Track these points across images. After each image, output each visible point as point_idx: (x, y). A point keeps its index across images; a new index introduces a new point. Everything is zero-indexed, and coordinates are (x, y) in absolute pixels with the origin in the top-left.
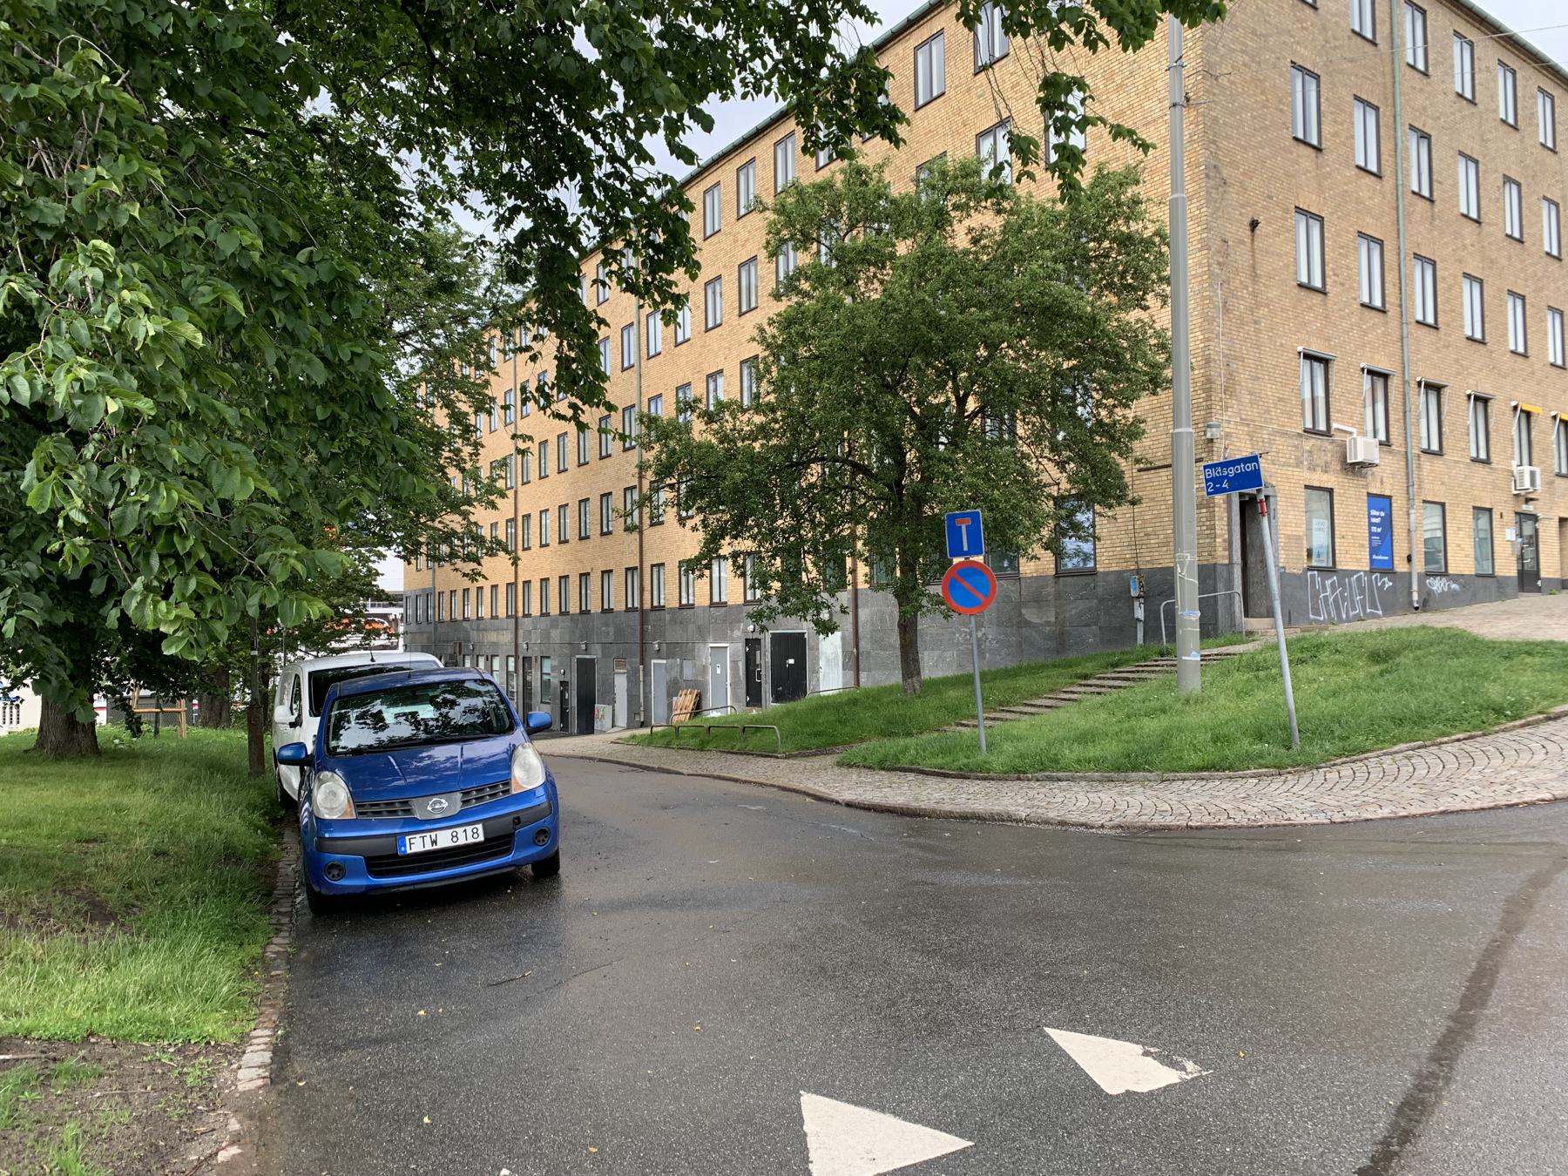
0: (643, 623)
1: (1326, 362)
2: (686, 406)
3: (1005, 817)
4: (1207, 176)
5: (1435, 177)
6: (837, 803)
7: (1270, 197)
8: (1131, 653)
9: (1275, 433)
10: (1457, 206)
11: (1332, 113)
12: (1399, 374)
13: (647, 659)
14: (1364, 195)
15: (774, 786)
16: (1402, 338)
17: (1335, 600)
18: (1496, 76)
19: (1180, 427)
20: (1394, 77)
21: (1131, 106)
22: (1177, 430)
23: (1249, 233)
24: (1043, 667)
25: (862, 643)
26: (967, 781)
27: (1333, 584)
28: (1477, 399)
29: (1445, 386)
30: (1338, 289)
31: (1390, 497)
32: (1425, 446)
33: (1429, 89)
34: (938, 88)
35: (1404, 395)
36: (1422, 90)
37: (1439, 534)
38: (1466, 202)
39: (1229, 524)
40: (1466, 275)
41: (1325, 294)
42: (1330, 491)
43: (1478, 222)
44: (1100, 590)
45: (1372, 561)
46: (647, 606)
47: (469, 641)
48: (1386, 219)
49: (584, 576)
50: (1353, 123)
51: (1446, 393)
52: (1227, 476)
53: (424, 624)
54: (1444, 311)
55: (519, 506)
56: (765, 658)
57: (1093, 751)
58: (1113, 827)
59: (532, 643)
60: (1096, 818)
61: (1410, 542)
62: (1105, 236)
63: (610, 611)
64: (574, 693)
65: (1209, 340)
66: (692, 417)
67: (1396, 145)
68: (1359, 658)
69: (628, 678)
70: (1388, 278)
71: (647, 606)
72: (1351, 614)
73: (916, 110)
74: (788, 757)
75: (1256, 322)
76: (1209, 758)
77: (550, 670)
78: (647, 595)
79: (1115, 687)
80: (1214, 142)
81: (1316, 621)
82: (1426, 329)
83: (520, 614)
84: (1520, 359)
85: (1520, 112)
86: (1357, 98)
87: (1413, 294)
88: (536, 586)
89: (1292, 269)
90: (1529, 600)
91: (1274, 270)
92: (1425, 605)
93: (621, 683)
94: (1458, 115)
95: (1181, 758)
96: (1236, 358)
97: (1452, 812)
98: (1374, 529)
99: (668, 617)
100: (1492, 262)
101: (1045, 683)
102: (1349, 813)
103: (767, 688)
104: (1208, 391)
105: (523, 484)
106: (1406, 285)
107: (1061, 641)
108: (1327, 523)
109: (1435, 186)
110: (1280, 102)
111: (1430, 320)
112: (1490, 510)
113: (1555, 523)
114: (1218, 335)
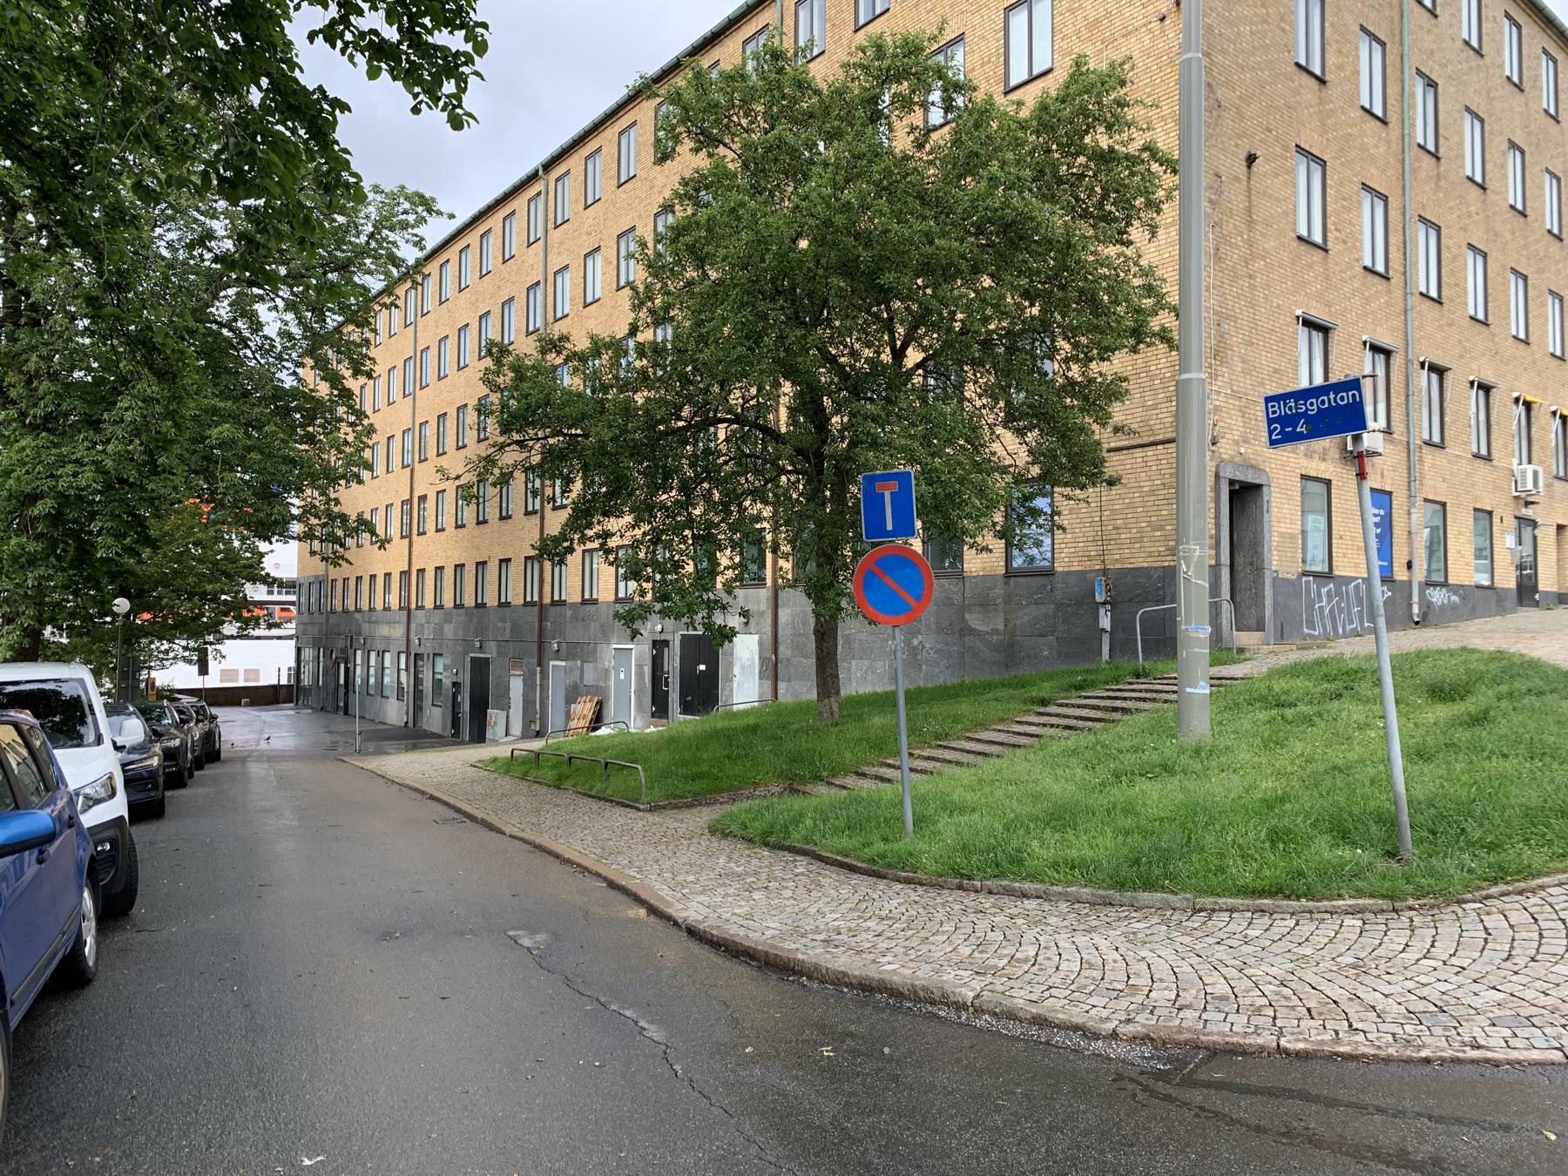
0: (542, 618)
1: (1325, 330)
2: (552, 345)
3: (937, 995)
5: (1441, 131)
6: (676, 923)
7: (1270, 131)
8: (1097, 671)
11: (1336, 41)
12: (1402, 352)
13: (545, 659)
14: (1370, 141)
15: (598, 875)
16: (1406, 311)
17: (1332, 611)
18: (1502, 28)
21: (1108, 14)
23: (1245, 169)
24: (989, 686)
25: (781, 649)
26: (882, 884)
27: (1329, 592)
28: (1481, 386)
29: (1448, 369)
30: (1341, 247)
31: (1390, 493)
32: (1426, 437)
34: (882, 4)
35: (1407, 377)
36: (1429, 31)
38: (1471, 166)
39: (1217, 517)
40: (1471, 246)
41: (1326, 251)
42: (1328, 483)
43: (1483, 188)
44: (1058, 595)
46: (547, 600)
47: (360, 634)
48: (1391, 172)
49: (481, 565)
50: (1358, 57)
51: (1449, 376)
52: (1305, 414)
53: (316, 614)
54: (1448, 284)
55: (415, 486)
56: (673, 662)
57: (1079, 849)
58: (1133, 1039)
59: (426, 633)
60: (1099, 1012)
61: (1410, 545)
62: (1081, 150)
63: (507, 604)
64: (467, 695)
66: (553, 359)
69: (524, 681)
70: (1392, 240)
71: (547, 600)
73: (856, 31)
74: (653, 809)
75: (1250, 277)
77: (443, 670)
78: (547, 588)
82: (1429, 303)
83: (413, 606)
84: (1522, 346)
85: (1525, 71)
90: (1528, 617)
93: (516, 686)
94: (1465, 65)
95: (1221, 870)
99: (569, 613)
100: (1496, 235)
101: (996, 710)
107: (1010, 651)
108: (1323, 519)
112: (1490, 513)
113: (1553, 530)
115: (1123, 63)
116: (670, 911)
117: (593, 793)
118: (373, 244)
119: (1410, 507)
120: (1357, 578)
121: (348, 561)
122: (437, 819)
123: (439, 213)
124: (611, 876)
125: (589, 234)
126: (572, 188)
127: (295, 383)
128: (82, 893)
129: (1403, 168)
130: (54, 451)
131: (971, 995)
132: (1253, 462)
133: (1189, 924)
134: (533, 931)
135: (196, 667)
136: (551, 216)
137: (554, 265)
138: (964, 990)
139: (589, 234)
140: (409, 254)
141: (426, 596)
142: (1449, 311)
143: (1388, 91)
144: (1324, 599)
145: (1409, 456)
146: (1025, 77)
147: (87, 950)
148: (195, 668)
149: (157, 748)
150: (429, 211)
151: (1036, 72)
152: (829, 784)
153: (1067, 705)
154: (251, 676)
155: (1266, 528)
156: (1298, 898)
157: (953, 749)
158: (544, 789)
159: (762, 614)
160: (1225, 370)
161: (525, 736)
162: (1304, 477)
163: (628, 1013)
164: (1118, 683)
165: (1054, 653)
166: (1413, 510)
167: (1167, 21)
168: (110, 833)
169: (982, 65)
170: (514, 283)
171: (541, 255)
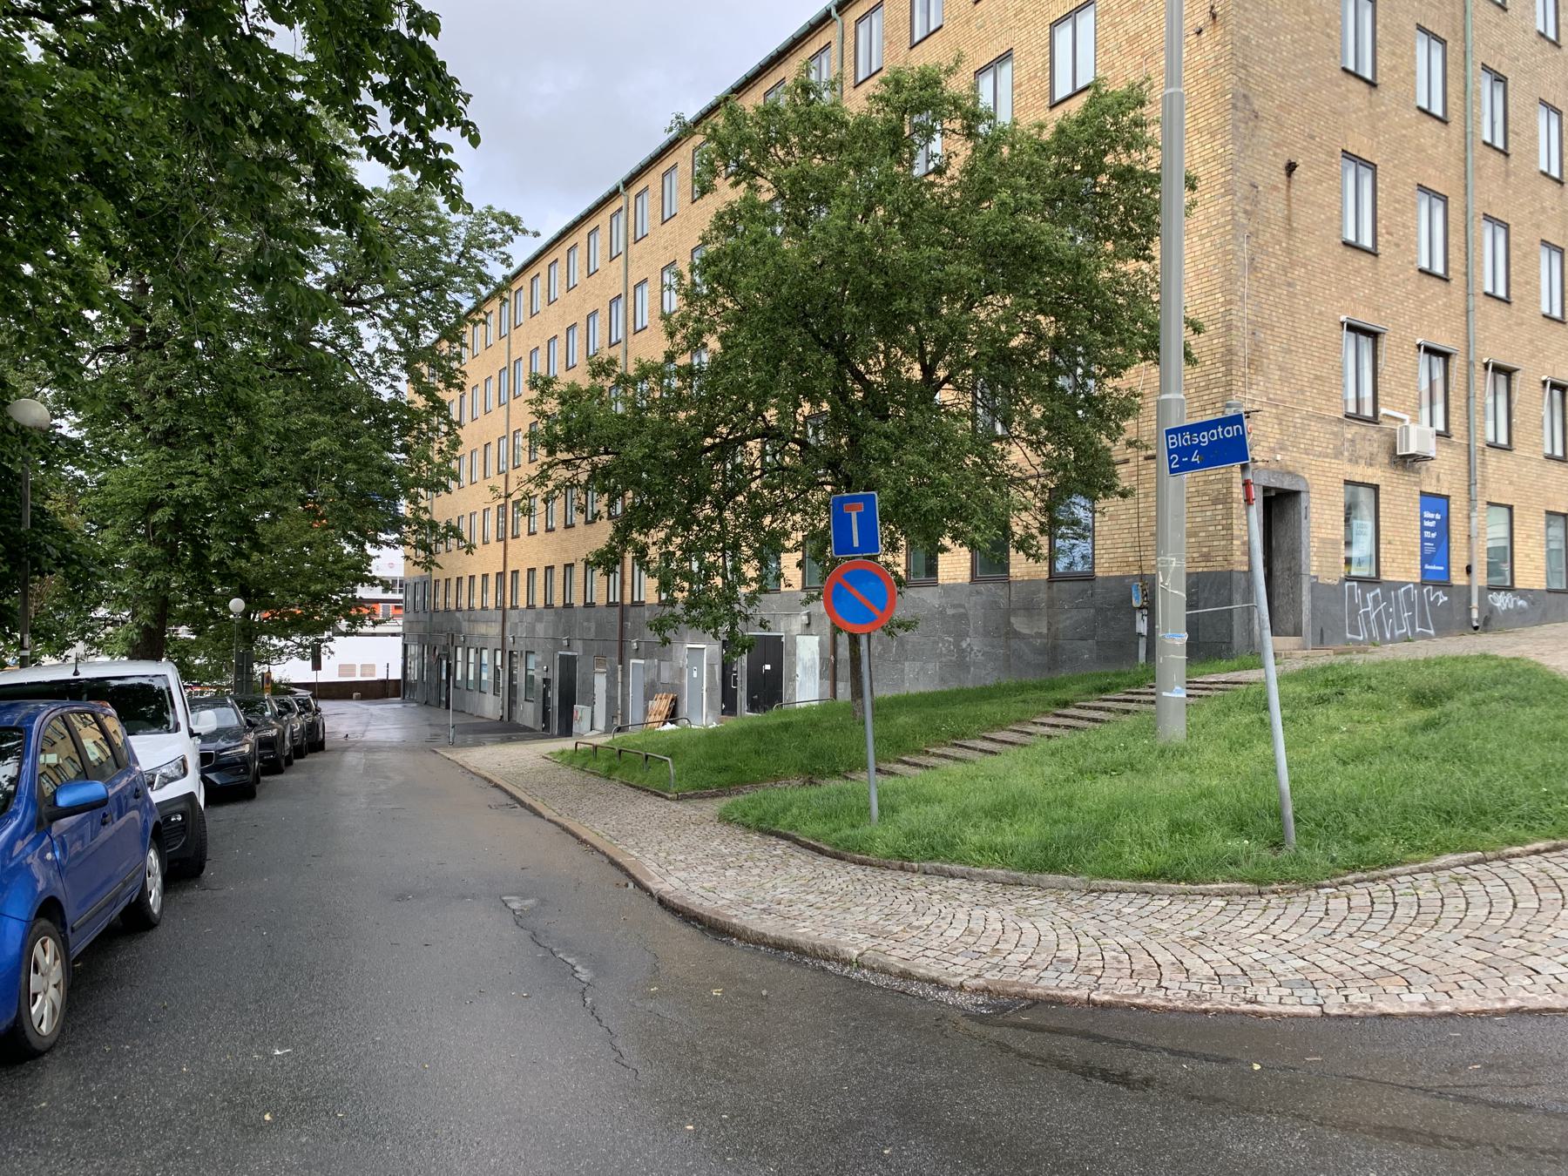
0: (623, 619)
1: (1374, 335)
3: (831, 952)
4: (1234, 107)
6: (651, 895)
7: (1313, 138)
9: (1310, 417)
10: (1536, 162)
14: (1427, 142)
15: (604, 853)
16: (1467, 312)
17: (1378, 616)
19: (1168, 391)
20: (1465, 7)
22: (1163, 397)
23: (1284, 177)
27: (1375, 598)
29: (1516, 370)
30: (1393, 250)
31: (1447, 497)
32: (1491, 438)
33: (1505, 24)
35: (1468, 379)
37: (1506, 543)
40: (1545, 243)
41: (1376, 255)
42: (1376, 488)
45: (1424, 572)
46: (627, 601)
49: (569, 567)
51: (1518, 378)
54: (1519, 284)
60: (960, 970)
61: (1470, 549)
63: (592, 605)
64: (556, 691)
65: (1230, 302)
67: (1466, 86)
68: (1399, 698)
70: (1452, 240)
71: (627, 601)
72: (1397, 633)
73: (911, 48)
74: (680, 798)
76: (1160, 860)
79: (1095, 720)
80: (1244, 67)
81: (1354, 641)
82: (1496, 303)
83: (508, 606)
86: (1420, 28)
87: (1482, 261)
88: (523, 576)
89: (1336, 224)
91: (1314, 223)
92: (1488, 623)
93: (600, 682)
94: (1539, 57)
95: (1120, 856)
96: (1264, 326)
97: (1531, 1012)
98: (1427, 534)
102: (1357, 997)
103: (742, 695)
104: (1228, 363)
105: (514, 468)
106: (1474, 249)
107: (1053, 655)
109: (1511, 136)
110: (1327, 25)
111: (1501, 293)
114: (1242, 298)
115: (1142, 83)
116: (650, 884)
117: (633, 783)
118: (464, 262)
119: (1470, 511)
120: (1407, 583)
121: (438, 566)
122: (492, 804)
123: (525, 232)
124: (612, 855)
125: (666, 248)
126: (650, 205)
127: (393, 395)
128: (145, 854)
129: (1466, 167)
130: (173, 464)
131: (856, 952)
132: (1291, 469)
133: (1079, 902)
134: (525, 896)
135: (310, 661)
136: (631, 231)
137: (633, 281)
138: (851, 949)
139: (666, 248)
140: (497, 271)
141: (520, 596)
142: (1518, 310)
143: (1449, 89)
144: (1370, 604)
145: (1469, 460)
146: (1069, 91)
147: (151, 900)
148: (310, 663)
149: (251, 737)
150: (516, 230)
151: (1080, 86)
152: (847, 778)
153: (1084, 707)
154: (367, 671)
155: (1304, 533)
156: (1179, 881)
157: (966, 747)
158: (596, 779)
159: (821, 617)
160: (1260, 378)
161: (607, 731)
162: (1347, 482)
163: (569, 960)
164: (1138, 687)
165: (1094, 656)
166: (1473, 514)
167: (1204, 35)
168: (182, 806)
169: (1029, 80)
170: (598, 296)
171: (622, 269)
